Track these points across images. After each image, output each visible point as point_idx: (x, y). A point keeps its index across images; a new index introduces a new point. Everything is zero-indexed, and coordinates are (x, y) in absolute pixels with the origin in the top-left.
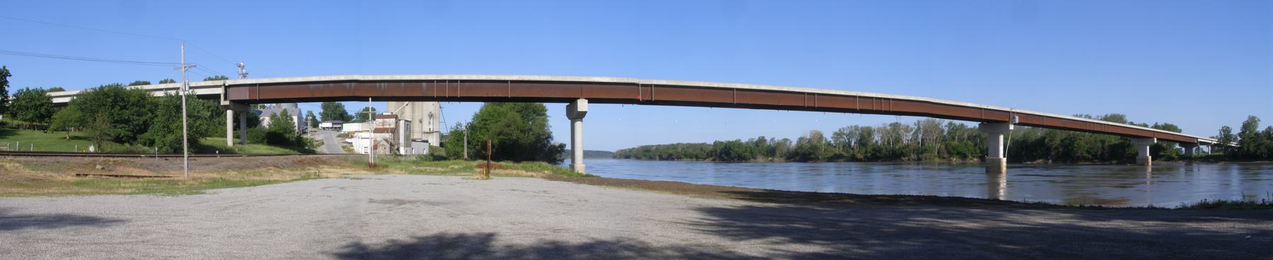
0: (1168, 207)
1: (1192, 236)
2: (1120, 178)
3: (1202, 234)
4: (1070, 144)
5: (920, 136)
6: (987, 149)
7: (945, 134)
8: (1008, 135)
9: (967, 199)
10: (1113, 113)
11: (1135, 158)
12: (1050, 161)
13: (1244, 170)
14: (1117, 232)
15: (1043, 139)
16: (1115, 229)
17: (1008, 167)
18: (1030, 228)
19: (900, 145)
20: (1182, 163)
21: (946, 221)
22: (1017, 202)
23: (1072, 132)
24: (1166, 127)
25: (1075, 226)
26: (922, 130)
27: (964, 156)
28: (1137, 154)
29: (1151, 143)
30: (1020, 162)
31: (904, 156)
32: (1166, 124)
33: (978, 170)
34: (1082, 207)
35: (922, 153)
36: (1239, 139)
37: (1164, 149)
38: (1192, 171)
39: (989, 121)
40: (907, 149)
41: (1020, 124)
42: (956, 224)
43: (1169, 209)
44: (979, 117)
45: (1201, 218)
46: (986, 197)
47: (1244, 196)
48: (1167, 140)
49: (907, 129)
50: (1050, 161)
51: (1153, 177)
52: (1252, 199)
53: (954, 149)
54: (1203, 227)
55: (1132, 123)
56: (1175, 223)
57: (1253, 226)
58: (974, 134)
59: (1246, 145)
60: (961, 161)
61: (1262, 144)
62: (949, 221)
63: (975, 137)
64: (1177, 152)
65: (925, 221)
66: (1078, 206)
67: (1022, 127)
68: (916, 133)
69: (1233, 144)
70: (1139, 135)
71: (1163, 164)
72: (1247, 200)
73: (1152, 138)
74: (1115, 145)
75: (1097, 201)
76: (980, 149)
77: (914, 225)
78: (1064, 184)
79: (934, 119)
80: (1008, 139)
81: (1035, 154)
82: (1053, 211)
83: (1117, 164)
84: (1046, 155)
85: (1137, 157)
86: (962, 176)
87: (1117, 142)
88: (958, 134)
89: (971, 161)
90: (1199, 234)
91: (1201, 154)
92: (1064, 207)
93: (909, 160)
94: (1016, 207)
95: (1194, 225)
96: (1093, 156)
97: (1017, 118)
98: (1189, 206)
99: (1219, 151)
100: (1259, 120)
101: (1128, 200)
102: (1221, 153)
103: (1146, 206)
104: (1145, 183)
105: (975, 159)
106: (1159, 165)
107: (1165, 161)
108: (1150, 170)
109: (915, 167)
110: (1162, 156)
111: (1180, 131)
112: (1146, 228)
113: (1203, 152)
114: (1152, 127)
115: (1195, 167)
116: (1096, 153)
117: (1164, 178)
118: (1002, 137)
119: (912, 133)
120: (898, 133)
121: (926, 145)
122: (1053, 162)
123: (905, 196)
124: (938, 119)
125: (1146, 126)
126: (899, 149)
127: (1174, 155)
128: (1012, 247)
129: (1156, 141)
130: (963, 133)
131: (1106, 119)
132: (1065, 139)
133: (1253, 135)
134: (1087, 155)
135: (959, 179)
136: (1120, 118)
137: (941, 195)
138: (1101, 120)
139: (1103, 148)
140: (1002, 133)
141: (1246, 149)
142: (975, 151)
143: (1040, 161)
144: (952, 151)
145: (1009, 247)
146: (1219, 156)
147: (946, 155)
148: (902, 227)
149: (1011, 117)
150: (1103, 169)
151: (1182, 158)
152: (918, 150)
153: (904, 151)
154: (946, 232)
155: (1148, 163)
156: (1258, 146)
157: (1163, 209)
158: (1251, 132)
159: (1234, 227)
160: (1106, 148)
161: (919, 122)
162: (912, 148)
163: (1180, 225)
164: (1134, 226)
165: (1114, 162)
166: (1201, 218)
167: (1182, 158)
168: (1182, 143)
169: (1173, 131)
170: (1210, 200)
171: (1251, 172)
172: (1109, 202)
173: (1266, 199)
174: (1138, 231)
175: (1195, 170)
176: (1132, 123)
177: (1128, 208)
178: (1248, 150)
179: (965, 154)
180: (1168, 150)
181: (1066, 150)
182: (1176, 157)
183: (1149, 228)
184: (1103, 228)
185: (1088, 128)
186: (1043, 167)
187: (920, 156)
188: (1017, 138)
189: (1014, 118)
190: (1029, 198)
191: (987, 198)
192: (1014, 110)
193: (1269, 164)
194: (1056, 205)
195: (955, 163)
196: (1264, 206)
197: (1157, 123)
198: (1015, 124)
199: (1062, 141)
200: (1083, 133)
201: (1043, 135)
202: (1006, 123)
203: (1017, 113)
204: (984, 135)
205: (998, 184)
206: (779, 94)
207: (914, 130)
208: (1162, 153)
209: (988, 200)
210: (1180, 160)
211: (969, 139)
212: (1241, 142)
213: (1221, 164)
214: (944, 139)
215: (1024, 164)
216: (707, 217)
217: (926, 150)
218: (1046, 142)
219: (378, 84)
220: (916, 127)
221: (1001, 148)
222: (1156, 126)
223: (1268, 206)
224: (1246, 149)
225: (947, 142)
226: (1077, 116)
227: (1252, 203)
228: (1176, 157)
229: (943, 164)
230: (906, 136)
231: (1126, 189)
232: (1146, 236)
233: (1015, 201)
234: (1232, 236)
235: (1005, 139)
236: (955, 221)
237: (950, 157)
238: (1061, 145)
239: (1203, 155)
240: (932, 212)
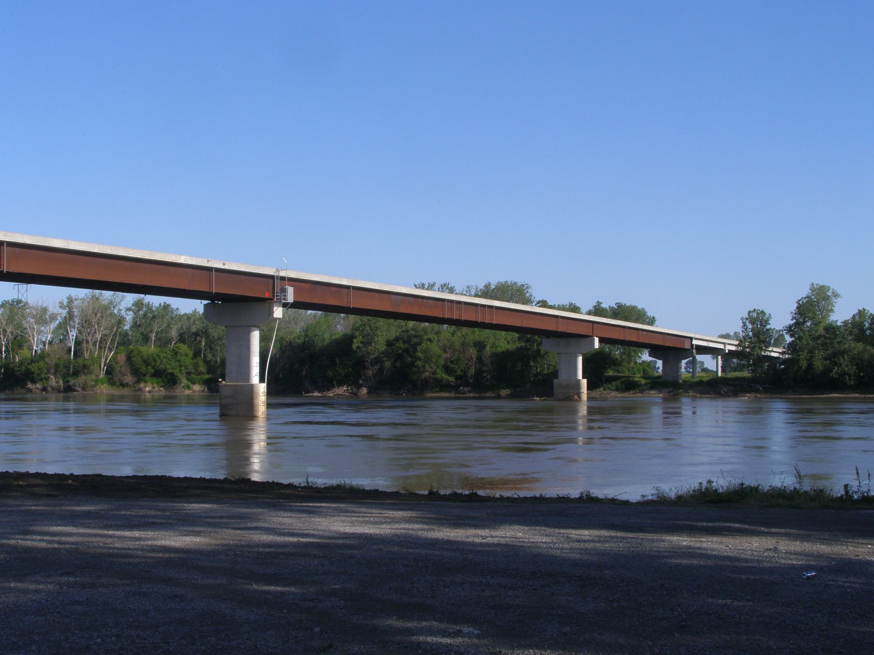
0: (623, 497)
1: (679, 565)
2: (517, 428)
3: (702, 562)
4: (406, 351)
5: (73, 334)
6: (223, 363)
7: (127, 327)
8: (271, 330)
9: (179, 479)
10: (502, 279)
11: (552, 383)
12: (364, 391)
13: (800, 412)
14: (512, 551)
15: (347, 339)
16: (506, 545)
17: (269, 405)
18: (318, 546)
19: (25, 353)
20: (656, 396)
21: (128, 533)
22: (290, 486)
23: (411, 324)
24: (621, 312)
25: (419, 538)
26: (77, 320)
27: (170, 381)
28: (555, 374)
29: (587, 350)
30: (297, 393)
31: (34, 381)
32: (620, 306)
33: (202, 411)
34: (433, 496)
35: (76, 374)
36: (788, 339)
37: (615, 363)
38: (678, 413)
39: (228, 299)
40: (42, 364)
41: (296, 305)
42: (153, 539)
43: (626, 503)
44: (204, 288)
45: (700, 524)
46: (220, 475)
47: (799, 476)
48: (623, 343)
49: (42, 316)
50: (364, 391)
51: (590, 428)
52: (820, 484)
53: (146, 363)
54: (704, 545)
55: (544, 304)
56: (641, 535)
57: (824, 549)
58: (194, 329)
59: (804, 355)
60: (163, 392)
61: (843, 353)
62: (137, 534)
63: (197, 334)
64: (644, 371)
65: (70, 534)
66: (426, 492)
67: (302, 311)
68: (63, 327)
69: (775, 352)
70: (561, 329)
71: (612, 396)
72: (807, 486)
73: (588, 337)
74: (507, 354)
75: (467, 481)
76: (207, 363)
77: (43, 545)
78: (392, 444)
79: (97, 292)
80: (270, 340)
81: (330, 373)
82: (370, 505)
83: (511, 397)
84: (353, 378)
85: (556, 381)
86: (166, 426)
87: (512, 347)
88: (156, 328)
89: (187, 392)
90: (695, 562)
91: (699, 374)
92: (395, 495)
93: (44, 389)
94: (288, 497)
95: (684, 541)
96: (458, 378)
97: (290, 290)
98: (673, 495)
99: (741, 368)
100: (836, 295)
101: (536, 480)
102: (746, 374)
103: (575, 493)
104: (573, 441)
105: (197, 388)
106: (605, 399)
107: (617, 390)
108: (583, 410)
109: (61, 405)
110: (610, 379)
111: (652, 322)
112: (575, 545)
113: (705, 370)
114: (589, 313)
115: (686, 405)
116: (465, 372)
117: (615, 430)
118: (255, 336)
119: (53, 325)
120: (19, 326)
121: (86, 355)
122: (369, 393)
123: (27, 475)
124: (107, 294)
125: (575, 309)
126: (21, 363)
127: (638, 378)
128: (279, 589)
129: (597, 345)
130: (169, 326)
131: (486, 293)
132: (397, 339)
133: (821, 331)
134: (445, 376)
135: (159, 433)
136: (516, 292)
137: (118, 474)
138: (476, 296)
139: (480, 359)
140: (257, 327)
141: (804, 364)
142: (196, 366)
143: (342, 390)
144: (143, 369)
145: (272, 588)
146: (743, 379)
147: (129, 379)
148: (14, 549)
149: (277, 289)
150: (480, 409)
151: (656, 383)
152: (67, 367)
153: (33, 368)
154: (127, 560)
155: (579, 394)
156: (833, 358)
157: (613, 501)
158: (817, 324)
159: (776, 549)
160: (488, 361)
161: (70, 300)
162: (52, 361)
163: (652, 540)
164: (548, 539)
165: (504, 392)
166: (700, 524)
167: (656, 383)
168: (656, 350)
169: (636, 321)
170: (721, 483)
171: (818, 419)
172: (492, 484)
173: (854, 485)
174: (557, 553)
175: (687, 412)
176: (544, 304)
177: (534, 498)
178: (810, 366)
179: (172, 374)
180: (625, 364)
181: (398, 365)
182: (643, 381)
183: (582, 545)
184: (481, 544)
185: (447, 316)
186: (349, 405)
187: (72, 381)
188: (289, 338)
189: (284, 291)
190: (318, 475)
191: (222, 477)
192: (282, 274)
193: (864, 401)
194: (376, 491)
195: (148, 396)
196: (847, 501)
197: (599, 303)
198: (285, 305)
199: (389, 344)
200: (435, 326)
201: (349, 331)
202: (265, 302)
203: (292, 281)
204: (217, 331)
205: (248, 445)
206: (377, 295)
207: (59, 319)
208: (611, 373)
209: (226, 480)
210: (652, 387)
211: (182, 339)
212: (792, 348)
213: (746, 398)
214: (124, 340)
215: (307, 397)
216: (208, 412)
217: (85, 367)
218: (354, 347)
219: (420, 300)
220: (64, 312)
221: (255, 360)
222: (598, 311)
223: (857, 501)
224: (804, 364)
225: (131, 347)
226: (422, 286)
227: (820, 494)
228: (643, 381)
229: (122, 398)
230: (40, 332)
231: (532, 455)
232: (574, 563)
233: (285, 481)
234: (772, 570)
235: (264, 340)
236: (150, 534)
237: (139, 381)
238: (386, 353)
239: (705, 377)
240: (88, 515)
